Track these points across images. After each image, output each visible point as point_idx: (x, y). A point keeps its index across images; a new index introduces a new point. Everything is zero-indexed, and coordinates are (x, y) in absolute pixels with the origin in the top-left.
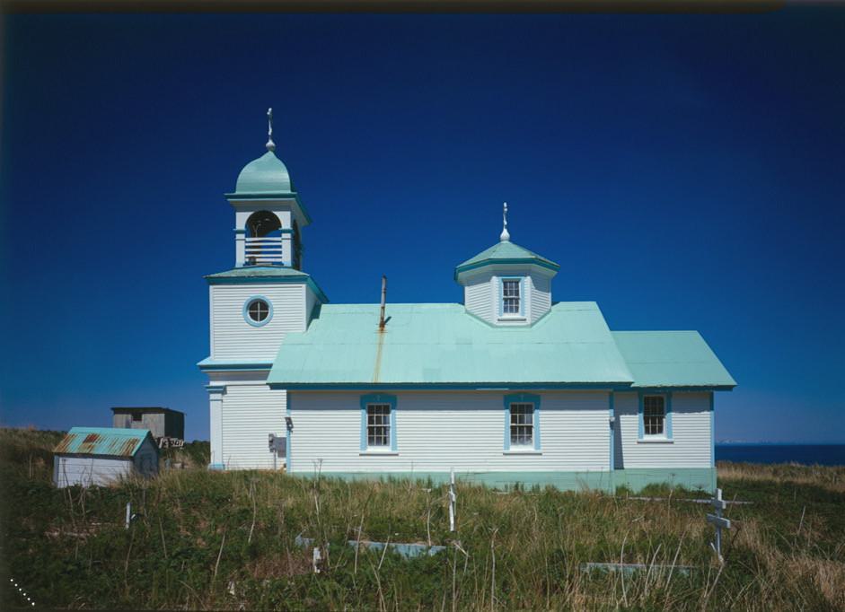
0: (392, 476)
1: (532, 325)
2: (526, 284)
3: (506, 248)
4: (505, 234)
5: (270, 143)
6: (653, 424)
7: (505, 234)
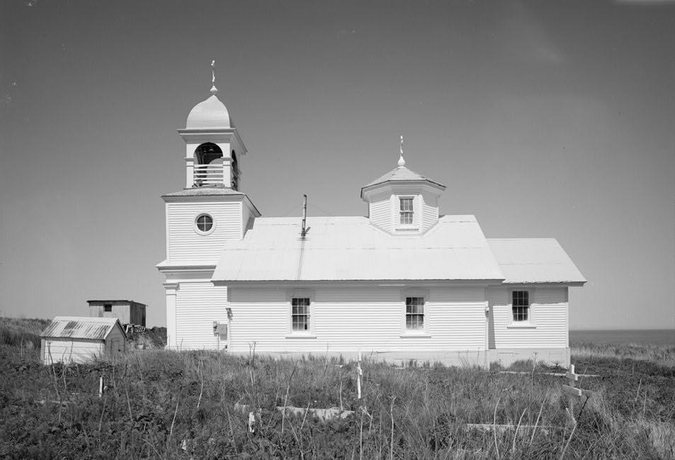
0: (313, 354)
1: (424, 233)
2: (418, 201)
3: (403, 172)
4: (402, 161)
5: (214, 89)
6: (520, 310)
7: (402, 161)
